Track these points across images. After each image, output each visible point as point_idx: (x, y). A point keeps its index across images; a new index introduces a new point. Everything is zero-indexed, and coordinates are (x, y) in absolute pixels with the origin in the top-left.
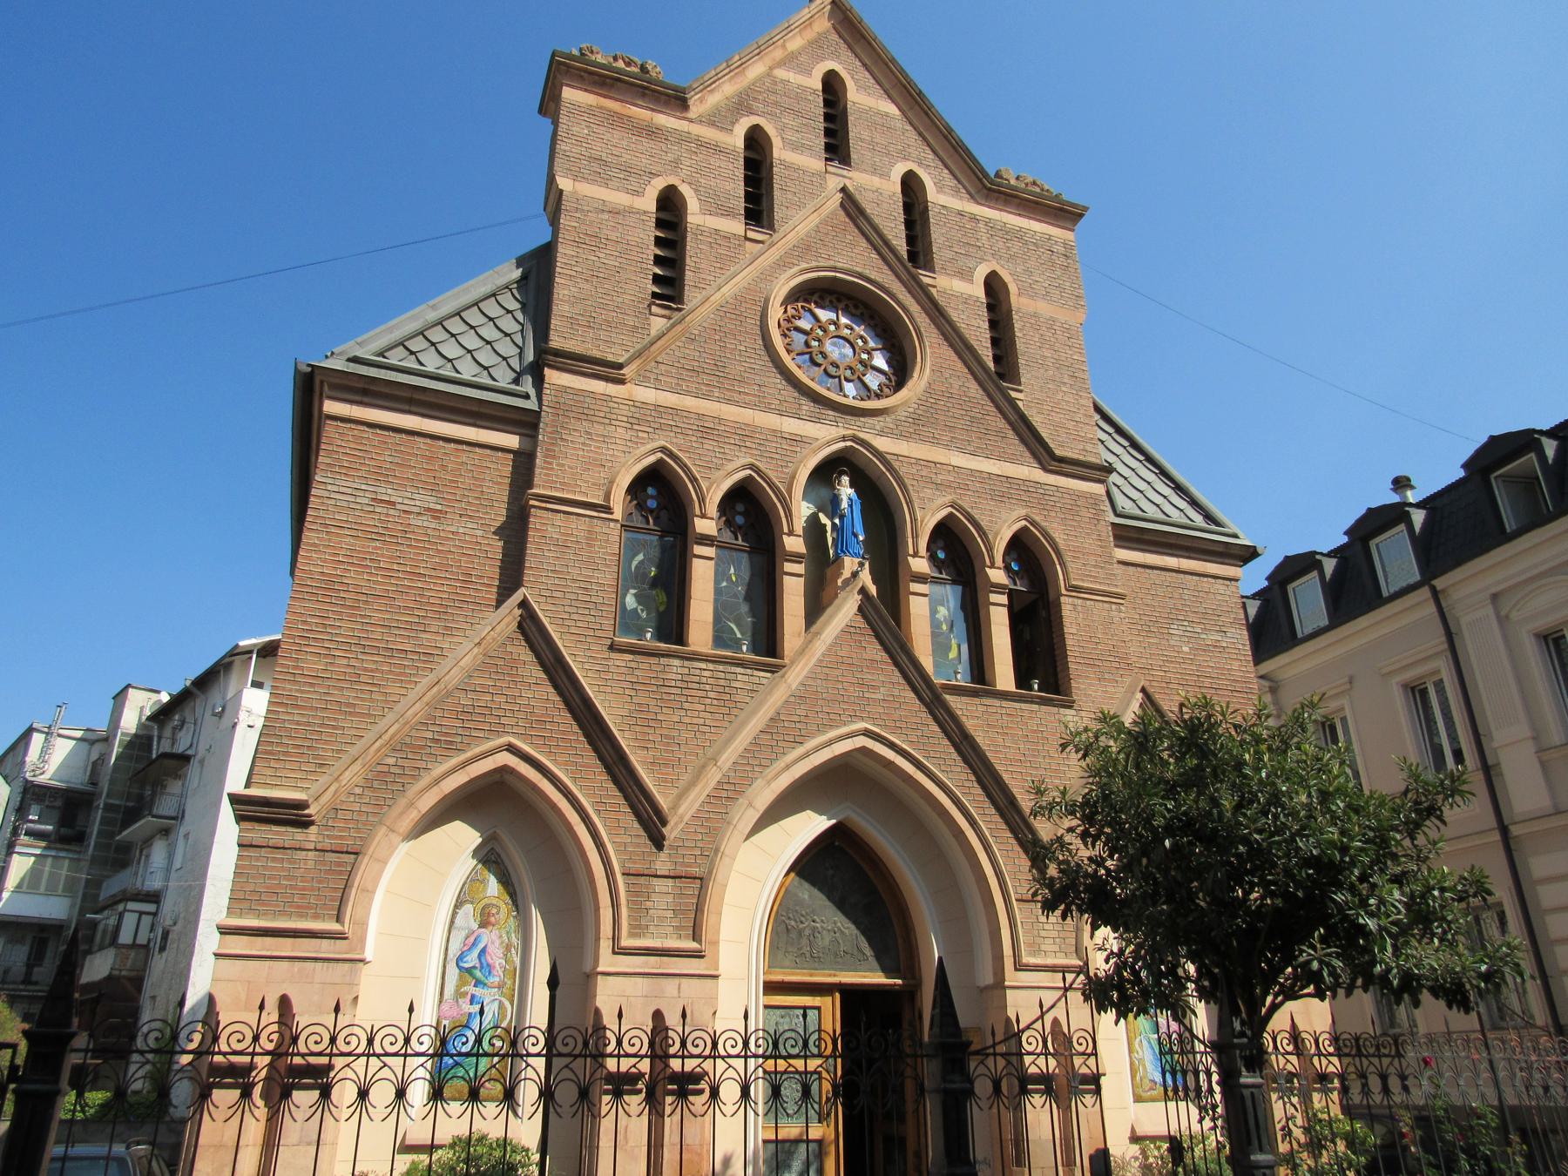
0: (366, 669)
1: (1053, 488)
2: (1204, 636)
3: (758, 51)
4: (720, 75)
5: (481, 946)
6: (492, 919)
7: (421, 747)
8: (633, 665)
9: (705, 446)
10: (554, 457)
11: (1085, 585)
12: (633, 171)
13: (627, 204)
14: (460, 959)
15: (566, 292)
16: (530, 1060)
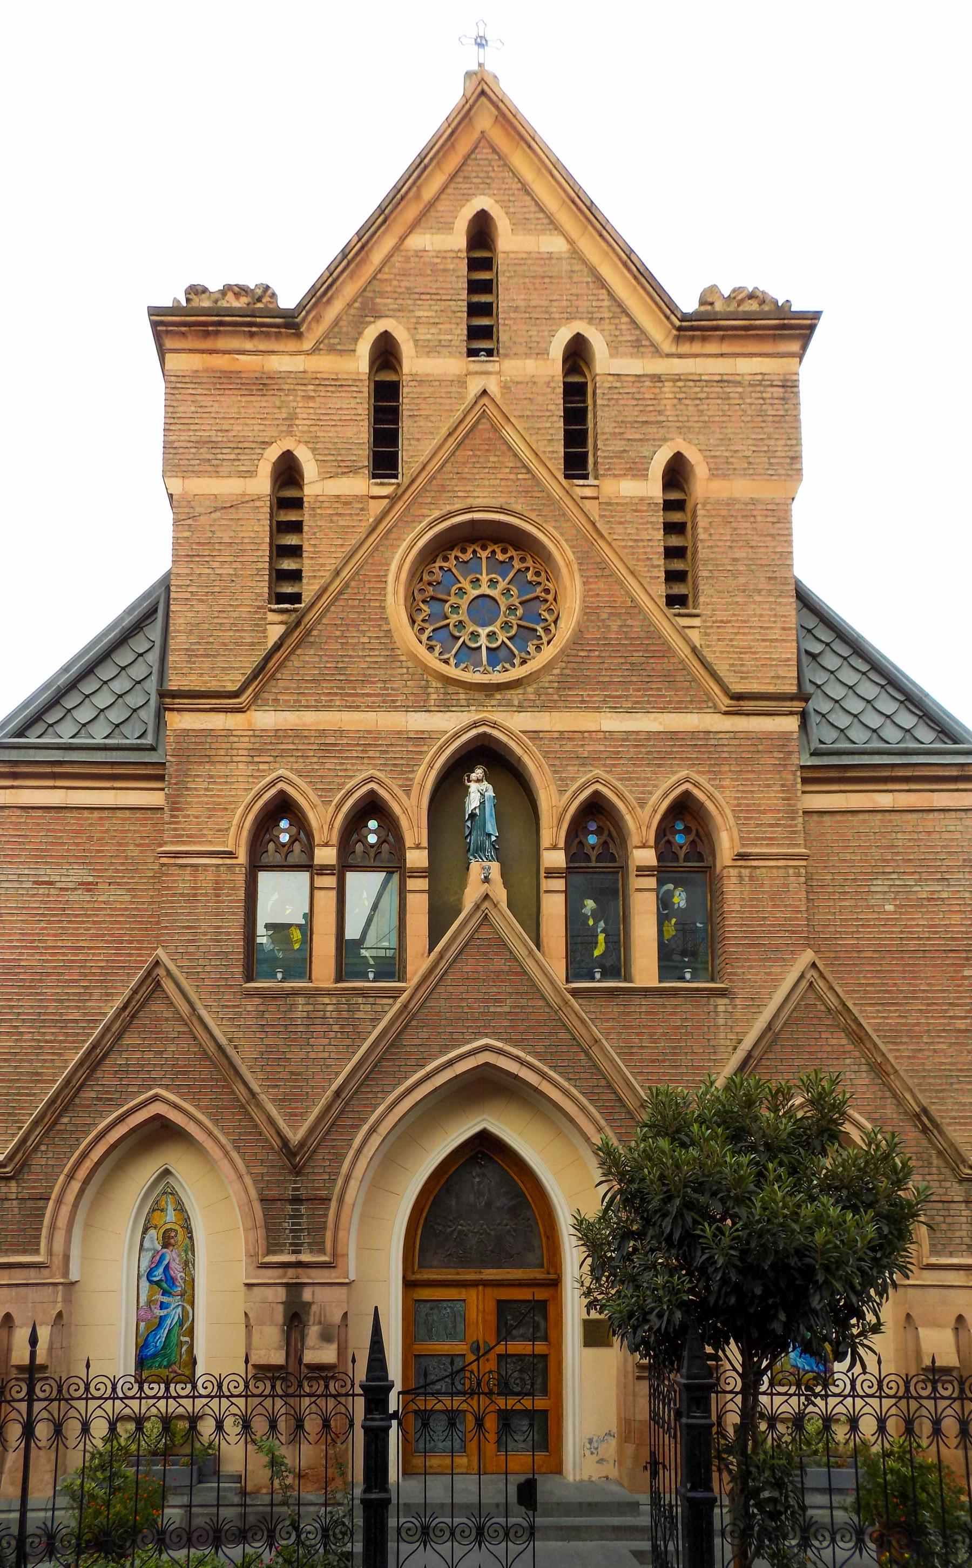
0: (47, 1042)
1: (728, 736)
2: (918, 889)
3: (382, 217)
4: (335, 275)
5: (165, 1262)
6: (172, 1241)
7: (88, 1106)
8: (261, 1008)
9: (327, 766)
10: (178, 809)
11: (757, 850)
12: (245, 445)
13: (239, 491)
14: (150, 1274)
15: (181, 621)
16: (15, 1404)
